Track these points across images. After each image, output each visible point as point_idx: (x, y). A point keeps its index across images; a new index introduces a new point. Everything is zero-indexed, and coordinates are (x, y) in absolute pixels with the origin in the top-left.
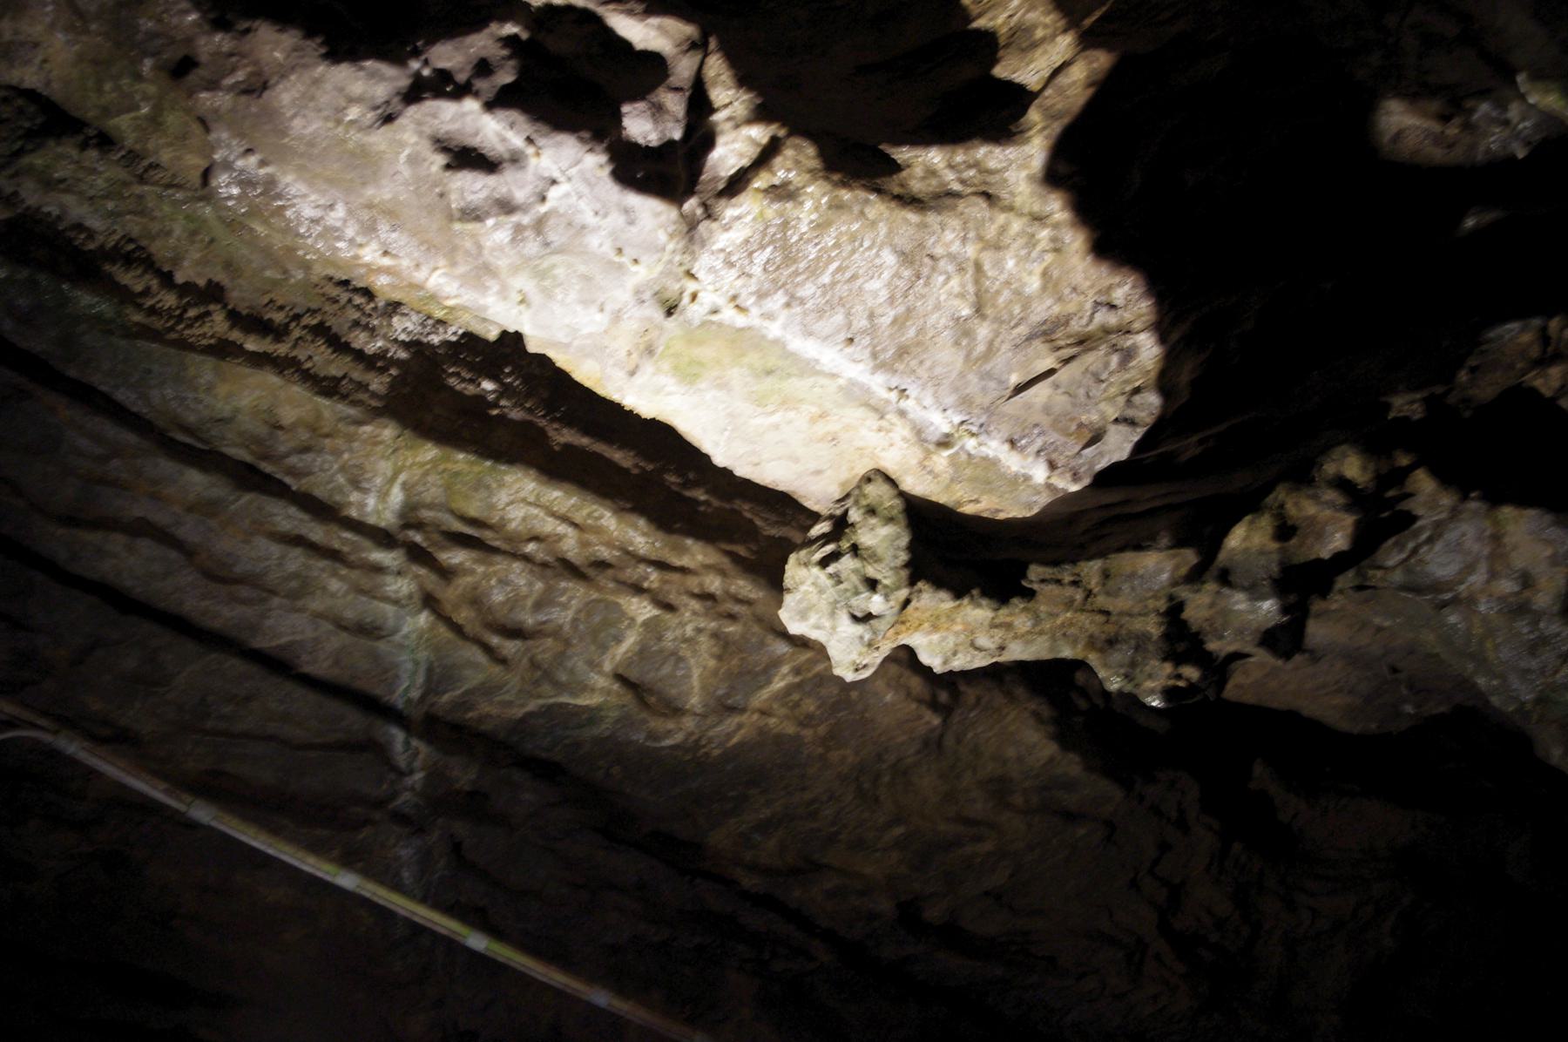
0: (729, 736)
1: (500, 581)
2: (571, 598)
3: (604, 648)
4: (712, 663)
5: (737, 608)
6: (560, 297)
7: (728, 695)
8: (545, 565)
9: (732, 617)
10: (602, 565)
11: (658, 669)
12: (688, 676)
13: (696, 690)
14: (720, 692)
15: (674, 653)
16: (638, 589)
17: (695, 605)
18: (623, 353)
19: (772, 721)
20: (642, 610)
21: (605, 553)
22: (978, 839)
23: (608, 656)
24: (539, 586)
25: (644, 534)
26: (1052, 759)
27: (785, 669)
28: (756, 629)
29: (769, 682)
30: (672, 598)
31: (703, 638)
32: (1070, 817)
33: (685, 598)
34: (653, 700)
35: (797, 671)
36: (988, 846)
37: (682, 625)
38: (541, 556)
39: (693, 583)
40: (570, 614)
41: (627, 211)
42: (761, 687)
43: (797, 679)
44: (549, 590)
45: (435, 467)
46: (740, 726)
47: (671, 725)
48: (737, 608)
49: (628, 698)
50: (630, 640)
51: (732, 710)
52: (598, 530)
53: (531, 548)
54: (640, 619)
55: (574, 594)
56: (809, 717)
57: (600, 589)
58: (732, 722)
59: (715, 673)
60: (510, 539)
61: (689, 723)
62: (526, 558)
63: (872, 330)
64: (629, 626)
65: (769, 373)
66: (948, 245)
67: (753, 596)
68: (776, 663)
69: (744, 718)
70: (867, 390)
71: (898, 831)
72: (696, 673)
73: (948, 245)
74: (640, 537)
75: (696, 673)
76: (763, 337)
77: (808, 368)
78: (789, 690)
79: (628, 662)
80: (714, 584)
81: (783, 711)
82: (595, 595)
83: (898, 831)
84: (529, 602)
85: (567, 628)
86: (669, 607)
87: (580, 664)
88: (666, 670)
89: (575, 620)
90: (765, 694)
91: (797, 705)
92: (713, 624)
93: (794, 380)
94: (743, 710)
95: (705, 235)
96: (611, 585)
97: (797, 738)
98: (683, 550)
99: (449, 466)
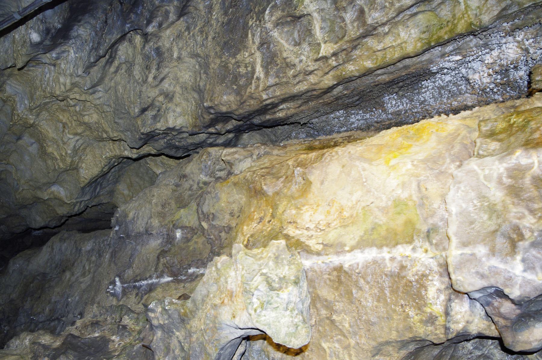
0: (253, 35)
1: (385, 7)
2: (354, 27)
3: (323, 20)
4: (285, 55)
5: (297, 80)
6: (475, 202)
7: (268, 48)
8: (375, 29)
9: (295, 76)
10: (355, 48)
11: (299, 32)
12: (287, 41)
13: (279, 39)
14: (272, 46)
15: (299, 44)
16: (335, 54)
17: (311, 69)
18: (428, 187)
19: (247, 54)
20: (326, 49)
21: (357, 52)
22: (155, 78)
23: (319, 18)
24: (370, 21)
25: (352, 71)
26: (167, 121)
27: (262, 76)
28: (284, 80)
29: (262, 66)
30: (320, 63)
31: (297, 60)
32: (144, 110)
33: (316, 67)
34: (289, 19)
35: (258, 79)
36: (150, 79)
37: (308, 57)
38: (380, 29)
39: (320, 73)
40: (348, 21)
41: (483, 276)
42: (262, 62)
43: (255, 77)
44: (364, 23)
45: (453, 24)
46: (254, 43)
47: (274, 18)
48: (297, 80)
49: (298, 14)
50: (318, 33)
51: (262, 44)
52: (368, 58)
53: (386, 29)
54: (323, 45)
55: (353, 31)
56: (239, 67)
57: (347, 42)
58: (257, 40)
59: (281, 52)
60: (396, 24)
61: (269, 25)
62: (384, 24)
63: (356, 283)
64: (323, 38)
65: (373, 229)
66: (361, 336)
67: (297, 87)
68: (267, 74)
69: (255, 47)
70: (338, 253)
71: (175, 55)
72: (286, 45)
73: (361, 336)
74: (351, 68)
75: (286, 45)
76: (387, 246)
77: (362, 244)
78: (253, 72)
79: (310, 23)
80: (312, 79)
81: (247, 61)
82: (346, 38)
83: (175, 55)
84: (366, 10)
85: (343, 15)
86: (317, 60)
87: (325, 6)
88: (296, 35)
89: (344, 20)
90: (259, 61)
91: (246, 67)
92: (298, 69)
93: (362, 233)
94: (258, 49)
95: (443, 279)
96: (345, 47)
97: (234, 56)
98: (334, 77)
99: (447, 29)
